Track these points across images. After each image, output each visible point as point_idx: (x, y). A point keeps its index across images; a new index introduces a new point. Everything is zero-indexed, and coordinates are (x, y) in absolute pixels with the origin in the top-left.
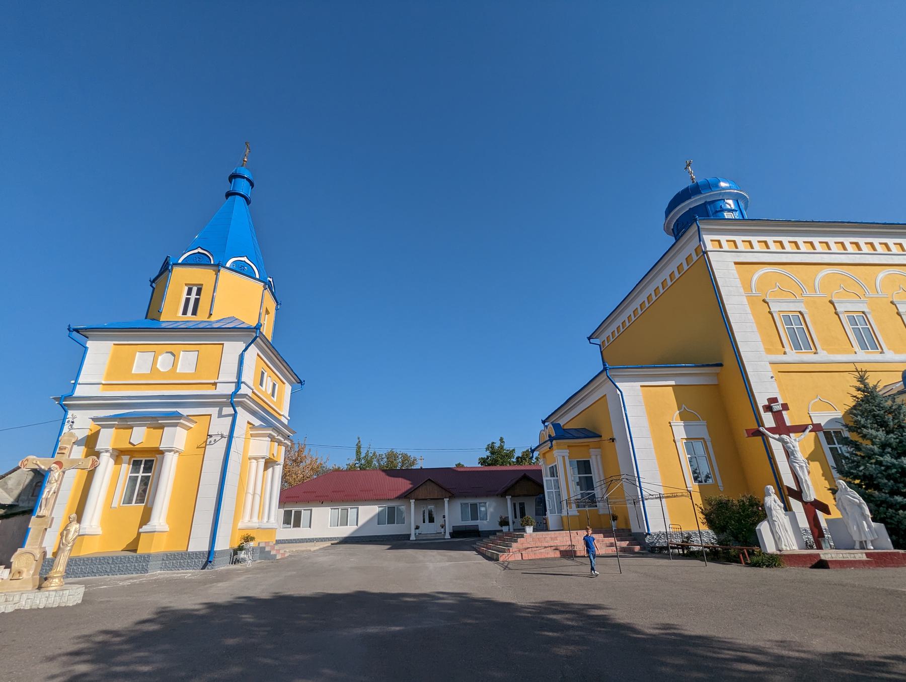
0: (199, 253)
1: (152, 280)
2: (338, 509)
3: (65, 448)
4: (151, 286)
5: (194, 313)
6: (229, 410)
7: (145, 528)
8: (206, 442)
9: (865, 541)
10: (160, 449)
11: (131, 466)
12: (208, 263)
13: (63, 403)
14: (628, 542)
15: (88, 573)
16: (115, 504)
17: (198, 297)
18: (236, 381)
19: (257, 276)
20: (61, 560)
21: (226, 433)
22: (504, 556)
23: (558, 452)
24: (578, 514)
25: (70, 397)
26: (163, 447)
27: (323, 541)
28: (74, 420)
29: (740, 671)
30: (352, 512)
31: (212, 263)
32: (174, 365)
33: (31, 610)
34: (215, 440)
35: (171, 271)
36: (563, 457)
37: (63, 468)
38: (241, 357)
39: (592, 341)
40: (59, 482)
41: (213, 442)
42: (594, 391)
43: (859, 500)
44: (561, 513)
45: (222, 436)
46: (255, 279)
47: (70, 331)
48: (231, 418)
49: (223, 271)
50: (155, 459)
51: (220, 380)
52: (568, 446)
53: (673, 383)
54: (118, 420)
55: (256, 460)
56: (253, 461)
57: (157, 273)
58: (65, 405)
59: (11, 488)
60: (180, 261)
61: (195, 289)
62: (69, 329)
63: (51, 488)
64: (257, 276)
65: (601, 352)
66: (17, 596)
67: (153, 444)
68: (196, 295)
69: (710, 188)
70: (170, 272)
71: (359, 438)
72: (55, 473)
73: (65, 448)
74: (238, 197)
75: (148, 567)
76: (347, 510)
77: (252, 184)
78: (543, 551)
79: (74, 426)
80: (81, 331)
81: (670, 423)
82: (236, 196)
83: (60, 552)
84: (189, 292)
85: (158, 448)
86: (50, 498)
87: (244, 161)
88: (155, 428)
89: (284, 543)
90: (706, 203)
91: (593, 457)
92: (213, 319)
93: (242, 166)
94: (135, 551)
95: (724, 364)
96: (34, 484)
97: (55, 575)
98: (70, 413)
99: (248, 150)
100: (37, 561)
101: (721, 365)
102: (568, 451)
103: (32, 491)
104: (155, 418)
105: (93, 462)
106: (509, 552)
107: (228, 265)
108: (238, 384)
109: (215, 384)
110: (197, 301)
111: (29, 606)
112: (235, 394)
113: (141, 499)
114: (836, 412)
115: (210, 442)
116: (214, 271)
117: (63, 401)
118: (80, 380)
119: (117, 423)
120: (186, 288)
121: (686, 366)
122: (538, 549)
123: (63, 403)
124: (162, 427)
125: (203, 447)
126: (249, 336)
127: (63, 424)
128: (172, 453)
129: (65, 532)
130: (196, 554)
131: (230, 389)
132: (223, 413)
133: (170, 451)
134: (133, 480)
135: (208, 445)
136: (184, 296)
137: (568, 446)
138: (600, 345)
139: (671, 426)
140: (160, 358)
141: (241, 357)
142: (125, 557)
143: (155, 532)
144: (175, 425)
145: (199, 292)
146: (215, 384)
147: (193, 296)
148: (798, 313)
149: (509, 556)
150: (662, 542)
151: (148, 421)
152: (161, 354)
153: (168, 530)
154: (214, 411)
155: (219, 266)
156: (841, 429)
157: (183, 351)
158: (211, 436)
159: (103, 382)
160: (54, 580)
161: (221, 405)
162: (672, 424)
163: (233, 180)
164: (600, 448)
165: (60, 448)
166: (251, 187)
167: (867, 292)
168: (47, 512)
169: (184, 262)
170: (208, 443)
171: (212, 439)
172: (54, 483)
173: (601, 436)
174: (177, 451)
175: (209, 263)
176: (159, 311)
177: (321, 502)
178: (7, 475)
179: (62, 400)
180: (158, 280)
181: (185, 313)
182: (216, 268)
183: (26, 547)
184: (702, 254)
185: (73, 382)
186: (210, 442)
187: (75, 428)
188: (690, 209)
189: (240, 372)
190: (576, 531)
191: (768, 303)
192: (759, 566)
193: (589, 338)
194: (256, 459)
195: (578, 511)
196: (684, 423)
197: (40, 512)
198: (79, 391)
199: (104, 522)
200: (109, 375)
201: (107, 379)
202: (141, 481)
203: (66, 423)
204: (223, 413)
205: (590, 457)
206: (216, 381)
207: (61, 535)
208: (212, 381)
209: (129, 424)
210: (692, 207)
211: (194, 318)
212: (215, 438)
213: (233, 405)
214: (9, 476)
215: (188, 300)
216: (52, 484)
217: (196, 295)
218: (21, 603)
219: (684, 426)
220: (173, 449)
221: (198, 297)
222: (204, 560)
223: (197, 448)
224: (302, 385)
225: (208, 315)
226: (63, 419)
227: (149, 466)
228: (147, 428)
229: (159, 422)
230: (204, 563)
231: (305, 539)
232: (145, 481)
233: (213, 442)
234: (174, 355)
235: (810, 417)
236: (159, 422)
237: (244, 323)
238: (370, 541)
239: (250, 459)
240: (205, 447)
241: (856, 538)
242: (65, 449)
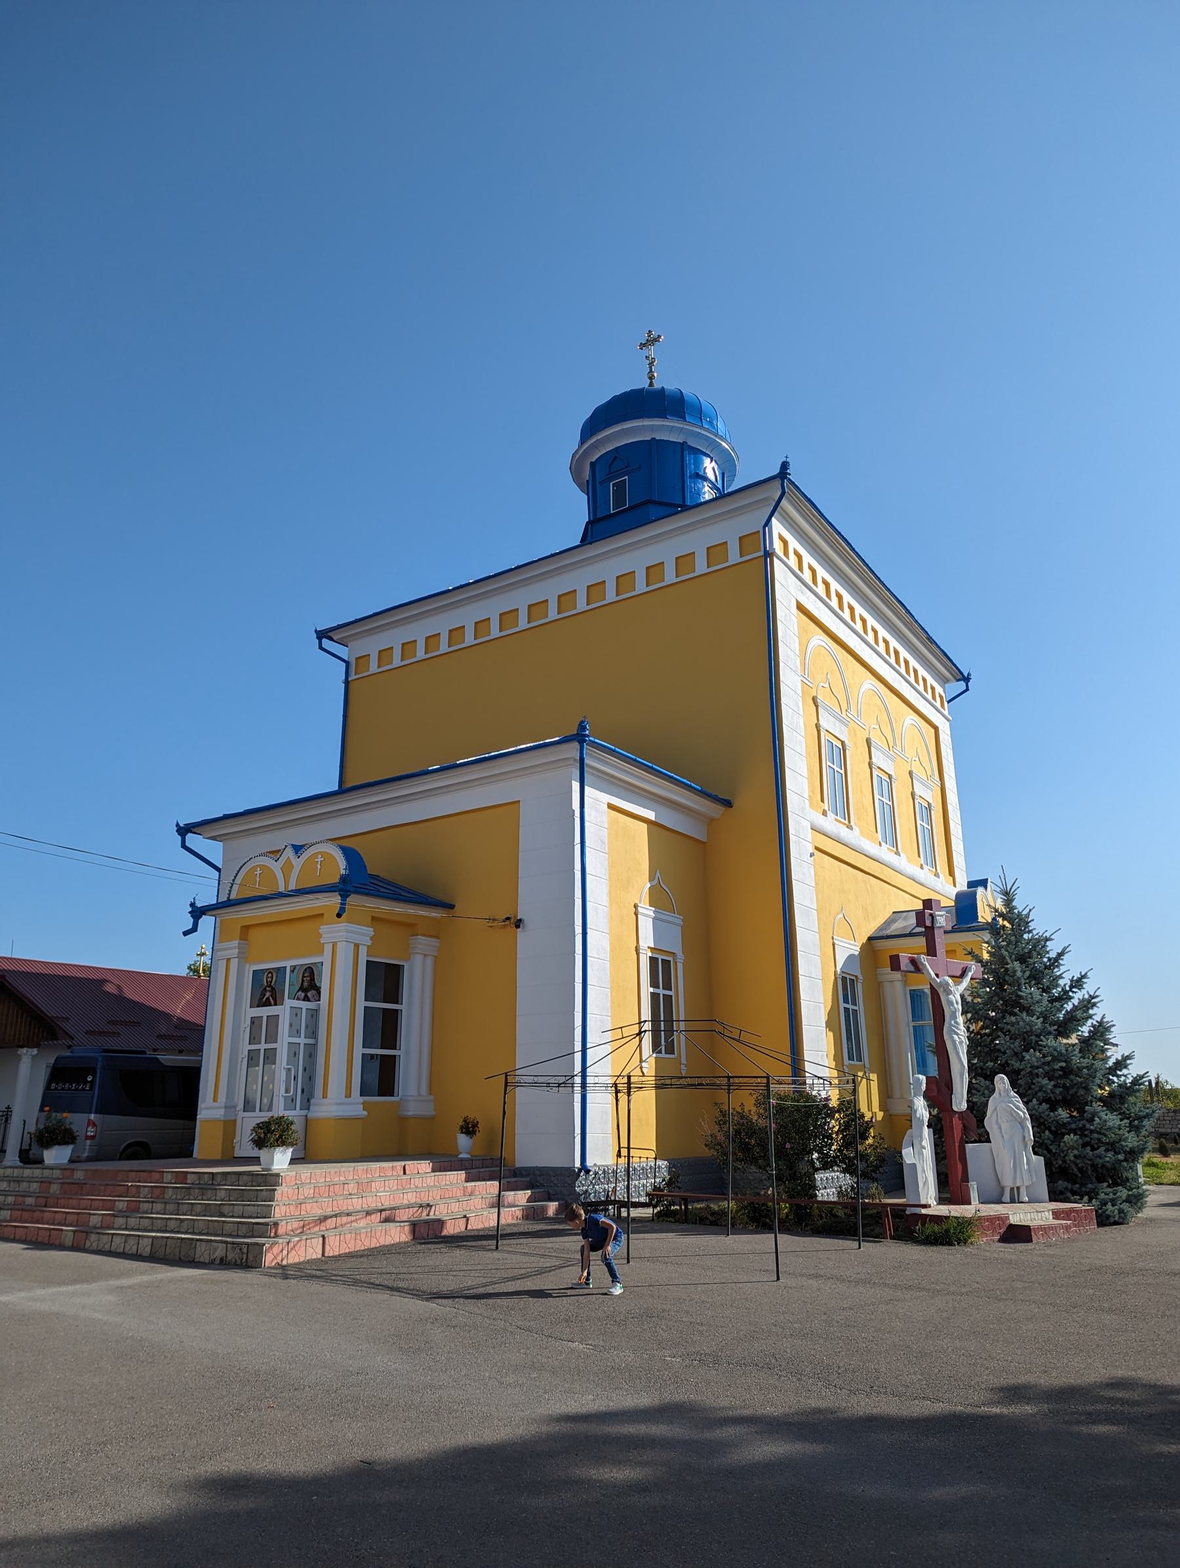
9: (1018, 1188)
14: (529, 1192)
22: (276, 1250)
23: (348, 931)
24: (365, 1113)
29: (640, 1464)
36: (357, 946)
39: (326, 643)
42: (453, 789)
43: (1024, 1113)
44: (308, 1109)
52: (373, 918)
53: (651, 815)
65: (347, 683)
69: (701, 418)
78: (362, 1223)
81: (636, 906)
90: (683, 445)
91: (418, 960)
95: (736, 804)
101: (728, 804)
102: (370, 931)
106: (276, 1236)
114: (853, 942)
121: (690, 786)
122: (350, 1218)
137: (373, 918)
138: (347, 663)
139: (636, 914)
148: (840, 742)
149: (291, 1245)
156: (856, 976)
162: (639, 909)
164: (438, 938)
167: (898, 743)
173: (452, 907)
183: (394, 662)
184: (762, 553)
188: (653, 439)
190: (403, 1163)
191: (817, 707)
192: (950, 1244)
193: (322, 635)
195: (365, 1106)
196: (654, 912)
205: (408, 958)
210: (658, 438)
219: (654, 919)
235: (834, 945)
241: (1008, 1183)
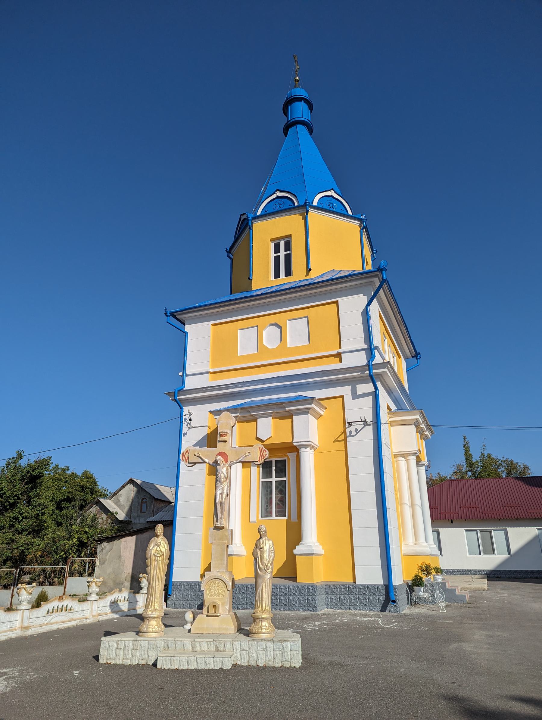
0: (278, 197)
1: (228, 249)
2: (476, 530)
3: (226, 434)
4: (229, 257)
5: (288, 273)
6: (369, 387)
7: (298, 550)
8: (345, 432)
10: (294, 444)
11: (261, 468)
12: (290, 207)
13: (178, 398)
15: (247, 604)
16: (253, 518)
17: (288, 252)
18: (366, 347)
19: (350, 213)
20: (264, 594)
21: (370, 418)
25: (181, 391)
26: (298, 440)
27: (463, 574)
28: (192, 417)
30: (498, 536)
31: (296, 204)
32: (282, 338)
33: (249, 667)
34: (356, 430)
35: (251, 228)
37: (229, 462)
38: (366, 314)
40: (228, 481)
41: (354, 433)
45: (365, 423)
46: (347, 216)
47: (167, 316)
48: (370, 399)
49: (313, 214)
50: (286, 459)
51: (344, 349)
54: (240, 411)
55: (404, 457)
56: (401, 458)
57: (233, 241)
58: (180, 399)
59: (123, 505)
60: (259, 213)
61: (282, 244)
62: (166, 314)
63: (223, 489)
64: (350, 213)
66: (228, 643)
67: (285, 439)
68: (285, 251)
70: (250, 229)
71: (465, 438)
72: (223, 468)
73: (226, 434)
74: (299, 126)
75: (315, 603)
76: (490, 532)
77: (311, 107)
79: (193, 424)
80: (178, 315)
82: (297, 125)
83: (260, 581)
84: (277, 249)
85: (292, 443)
86: (225, 502)
87: (296, 80)
88: (281, 418)
89: (455, 575)
92: (313, 275)
93: (295, 87)
94: (294, 578)
96: (140, 500)
97: (263, 616)
98: (186, 409)
99: (297, 67)
100: (229, 590)
103: (139, 507)
104: (281, 404)
105: (261, 452)
107: (315, 203)
108: (370, 350)
109: (339, 355)
110: (288, 258)
111: (246, 661)
112: (369, 366)
113: (281, 512)
115: (351, 432)
116: (300, 215)
117: (178, 396)
118: (188, 371)
119: (238, 414)
120: (272, 245)
123: (178, 398)
124: (290, 416)
125: (344, 438)
126: (371, 284)
127: (181, 422)
128: (308, 449)
129: (259, 551)
130: (378, 588)
131: (361, 359)
132: (359, 393)
133: (305, 446)
134: (267, 486)
135: (349, 436)
136: (272, 255)
140: (264, 333)
141: (366, 314)
142: (285, 587)
143: (312, 554)
144: (305, 412)
145: (288, 246)
146: (339, 355)
147: (282, 253)
150: (263, 561)
151: (273, 409)
152: (264, 328)
153: (323, 553)
154: (345, 391)
155: (306, 206)
157: (289, 320)
158: (350, 424)
159: (211, 370)
160: (263, 624)
161: (353, 382)
163: (289, 107)
165: (220, 435)
166: (310, 111)
168: (224, 522)
169: (263, 213)
170: (348, 434)
171: (352, 428)
172: (224, 481)
174: (313, 447)
175: (293, 206)
176: (249, 279)
177: (450, 521)
178: (118, 492)
179: (176, 395)
180: (235, 247)
181: (277, 275)
182: (303, 211)
185: (181, 374)
186: (351, 432)
187: (194, 426)
189: (369, 334)
194: (403, 455)
197: (217, 521)
198: (190, 383)
199: (321, 539)
200: (215, 361)
201: (213, 366)
202: (277, 488)
203: (184, 422)
204: (359, 393)
206: (340, 351)
207: (253, 555)
208: (335, 352)
209: (252, 415)
211: (289, 279)
212: (355, 427)
213: (372, 379)
214: (120, 493)
215: (277, 259)
216: (223, 483)
217: (285, 251)
218: (235, 655)
220: (310, 443)
221: (288, 252)
222: (382, 598)
223: (335, 441)
224: (417, 359)
225: (305, 272)
226: (181, 417)
227: (281, 469)
228: (273, 418)
229: (287, 409)
230: (383, 602)
231: (458, 571)
232: (282, 487)
233: (354, 433)
234: (279, 327)
236: (287, 409)
237: (355, 271)
238: (537, 578)
239: (395, 456)
240: (345, 440)
242: (226, 435)
